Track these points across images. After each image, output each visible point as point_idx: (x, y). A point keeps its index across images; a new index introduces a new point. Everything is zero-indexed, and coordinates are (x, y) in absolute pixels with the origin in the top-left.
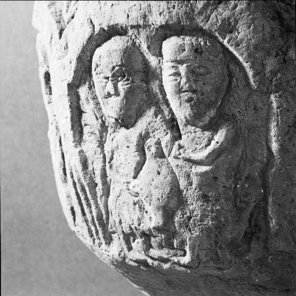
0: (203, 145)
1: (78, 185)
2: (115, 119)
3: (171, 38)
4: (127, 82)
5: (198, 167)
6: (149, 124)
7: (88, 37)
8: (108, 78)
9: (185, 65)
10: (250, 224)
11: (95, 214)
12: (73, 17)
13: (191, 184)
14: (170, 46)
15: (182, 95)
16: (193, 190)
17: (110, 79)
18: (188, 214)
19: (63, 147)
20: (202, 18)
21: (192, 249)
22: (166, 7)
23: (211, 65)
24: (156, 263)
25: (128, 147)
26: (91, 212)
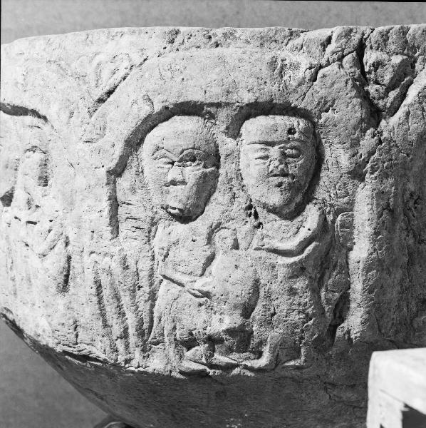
0: (291, 233)
1: (106, 292)
2: (179, 209)
3: (258, 118)
4: (198, 167)
5: (284, 258)
6: (223, 213)
7: (145, 116)
8: (172, 163)
9: (276, 147)
10: (335, 315)
11: (131, 321)
12: (124, 79)
13: (276, 276)
14: (255, 127)
15: (271, 179)
16: (279, 283)
17: (175, 164)
18: (272, 311)
19: (123, 83)
20: (297, 96)
21: (273, 350)
22: (256, 83)
23: (304, 147)
24: (218, 372)
25: (194, 241)
26: (122, 314)
